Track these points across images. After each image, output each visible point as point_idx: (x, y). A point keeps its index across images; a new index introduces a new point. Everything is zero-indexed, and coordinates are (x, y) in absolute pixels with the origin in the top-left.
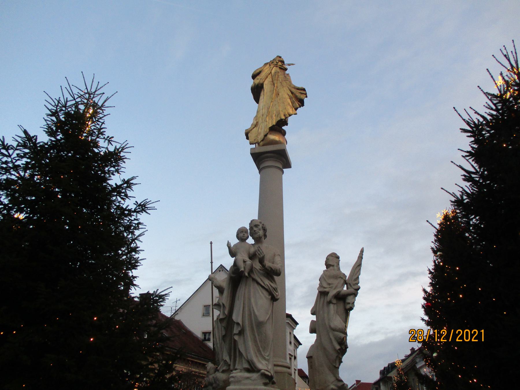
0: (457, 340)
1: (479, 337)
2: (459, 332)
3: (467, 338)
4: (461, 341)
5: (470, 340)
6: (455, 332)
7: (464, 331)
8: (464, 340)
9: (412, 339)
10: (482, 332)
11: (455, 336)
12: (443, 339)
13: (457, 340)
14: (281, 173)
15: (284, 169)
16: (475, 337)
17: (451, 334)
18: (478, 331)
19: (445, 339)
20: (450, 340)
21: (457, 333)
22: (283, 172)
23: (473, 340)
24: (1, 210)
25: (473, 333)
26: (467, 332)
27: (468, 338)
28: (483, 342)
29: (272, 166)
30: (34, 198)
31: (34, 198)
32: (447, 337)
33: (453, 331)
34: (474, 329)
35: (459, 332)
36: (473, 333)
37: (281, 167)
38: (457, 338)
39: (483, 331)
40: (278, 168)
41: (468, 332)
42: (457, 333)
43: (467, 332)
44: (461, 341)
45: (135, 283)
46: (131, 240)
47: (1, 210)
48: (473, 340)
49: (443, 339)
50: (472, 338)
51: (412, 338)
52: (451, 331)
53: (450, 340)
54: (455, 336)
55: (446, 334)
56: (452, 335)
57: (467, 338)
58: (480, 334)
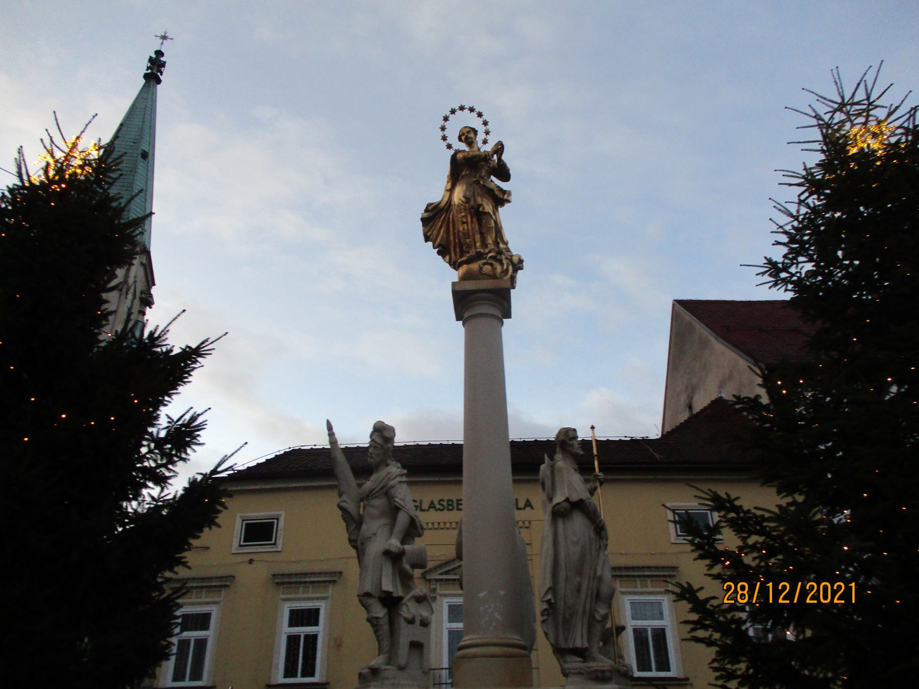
0: (808, 601)
1: (846, 595)
2: (812, 587)
3: (825, 598)
4: (815, 602)
5: (831, 600)
6: (803, 587)
7: (820, 585)
8: (820, 600)
9: (728, 599)
10: (851, 587)
11: (804, 593)
12: (838, 599)
13: (808, 601)
14: (499, 323)
15: (504, 320)
16: (840, 596)
17: (797, 589)
18: (845, 585)
19: (731, 600)
20: (795, 601)
21: (780, 588)
22: (502, 323)
23: (836, 601)
24: (146, 437)
25: (835, 588)
26: (825, 588)
27: (828, 598)
28: (854, 603)
29: (495, 316)
30: (830, 444)
31: (830, 444)
32: (790, 596)
33: (760, 584)
34: (837, 582)
35: (812, 587)
36: (835, 588)
37: (500, 315)
38: (807, 598)
39: (853, 585)
40: (492, 316)
41: (828, 587)
42: (780, 588)
43: (825, 588)
44: (815, 602)
45: (217, 521)
46: (162, 459)
47: (146, 437)
48: (836, 601)
49: (838, 599)
50: (834, 597)
51: (728, 598)
52: (798, 585)
53: (795, 601)
54: (804, 593)
55: (789, 590)
56: (800, 591)
57: (825, 598)
58: (848, 589)
